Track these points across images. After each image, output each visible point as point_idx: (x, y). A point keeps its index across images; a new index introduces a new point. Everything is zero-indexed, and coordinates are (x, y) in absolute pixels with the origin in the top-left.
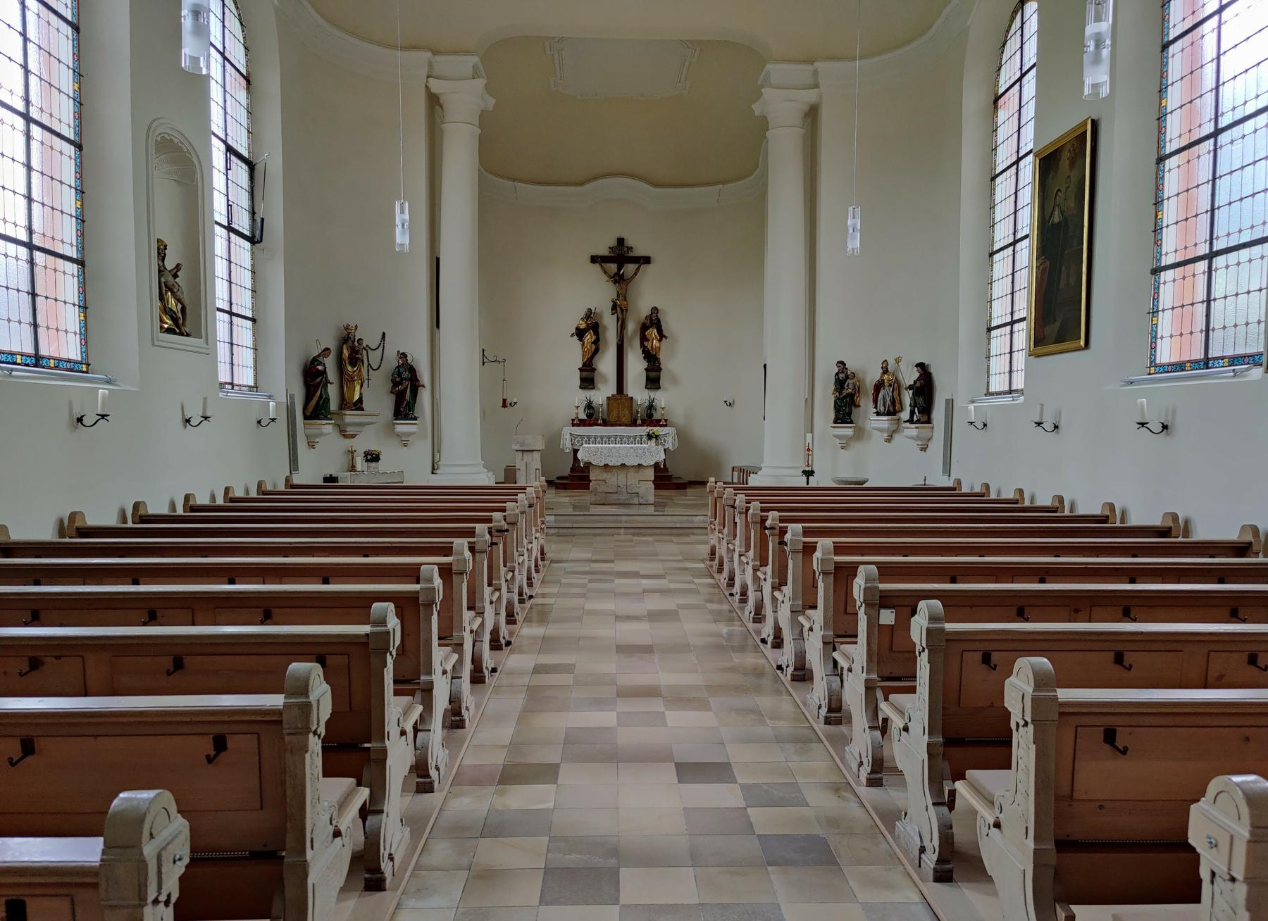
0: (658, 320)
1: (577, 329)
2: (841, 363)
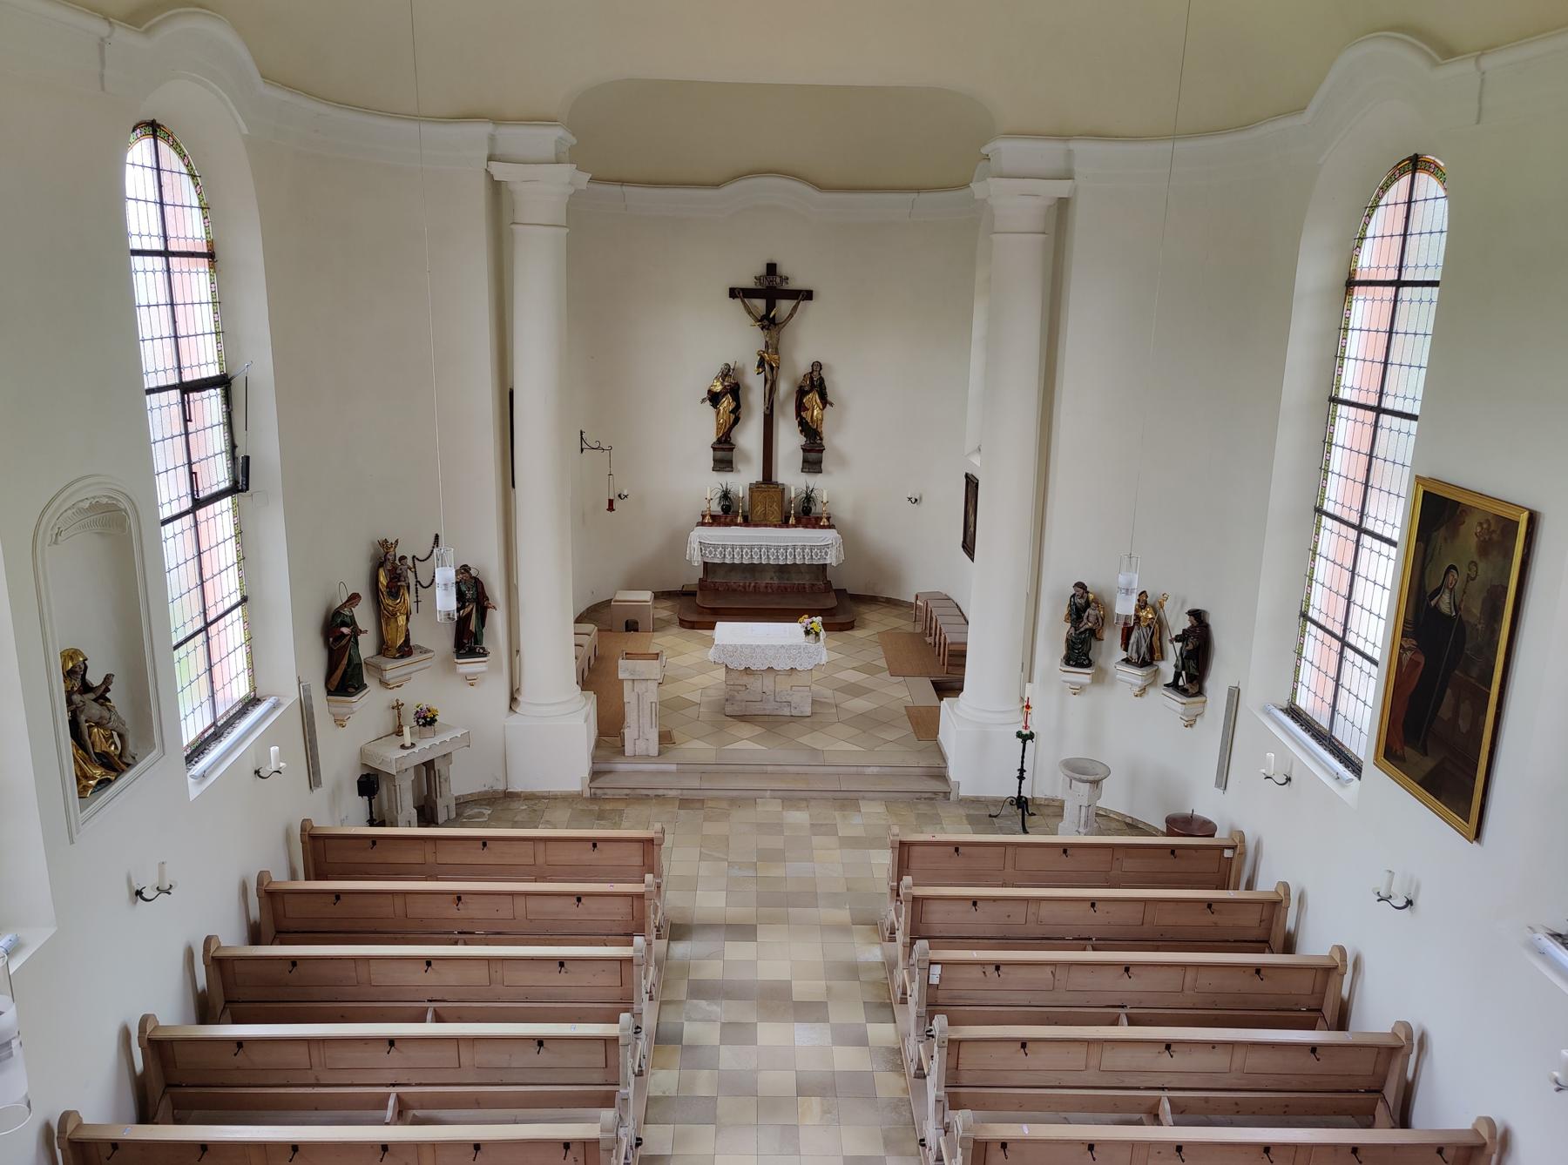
0: (822, 380)
1: (709, 391)
2: (1080, 586)
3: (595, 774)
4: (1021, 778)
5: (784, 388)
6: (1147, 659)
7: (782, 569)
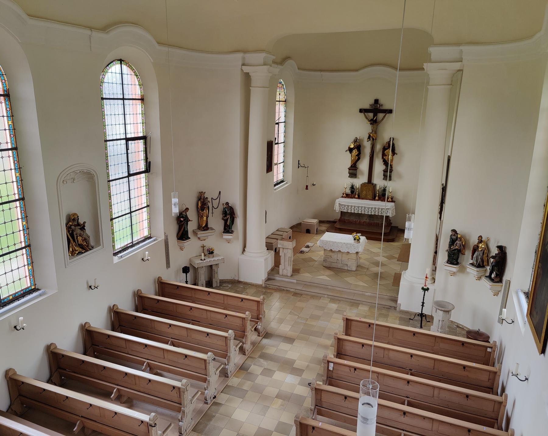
2: (454, 231)
3: (268, 279)
4: (423, 306)
5: (379, 147)
6: (480, 265)
7: (371, 216)
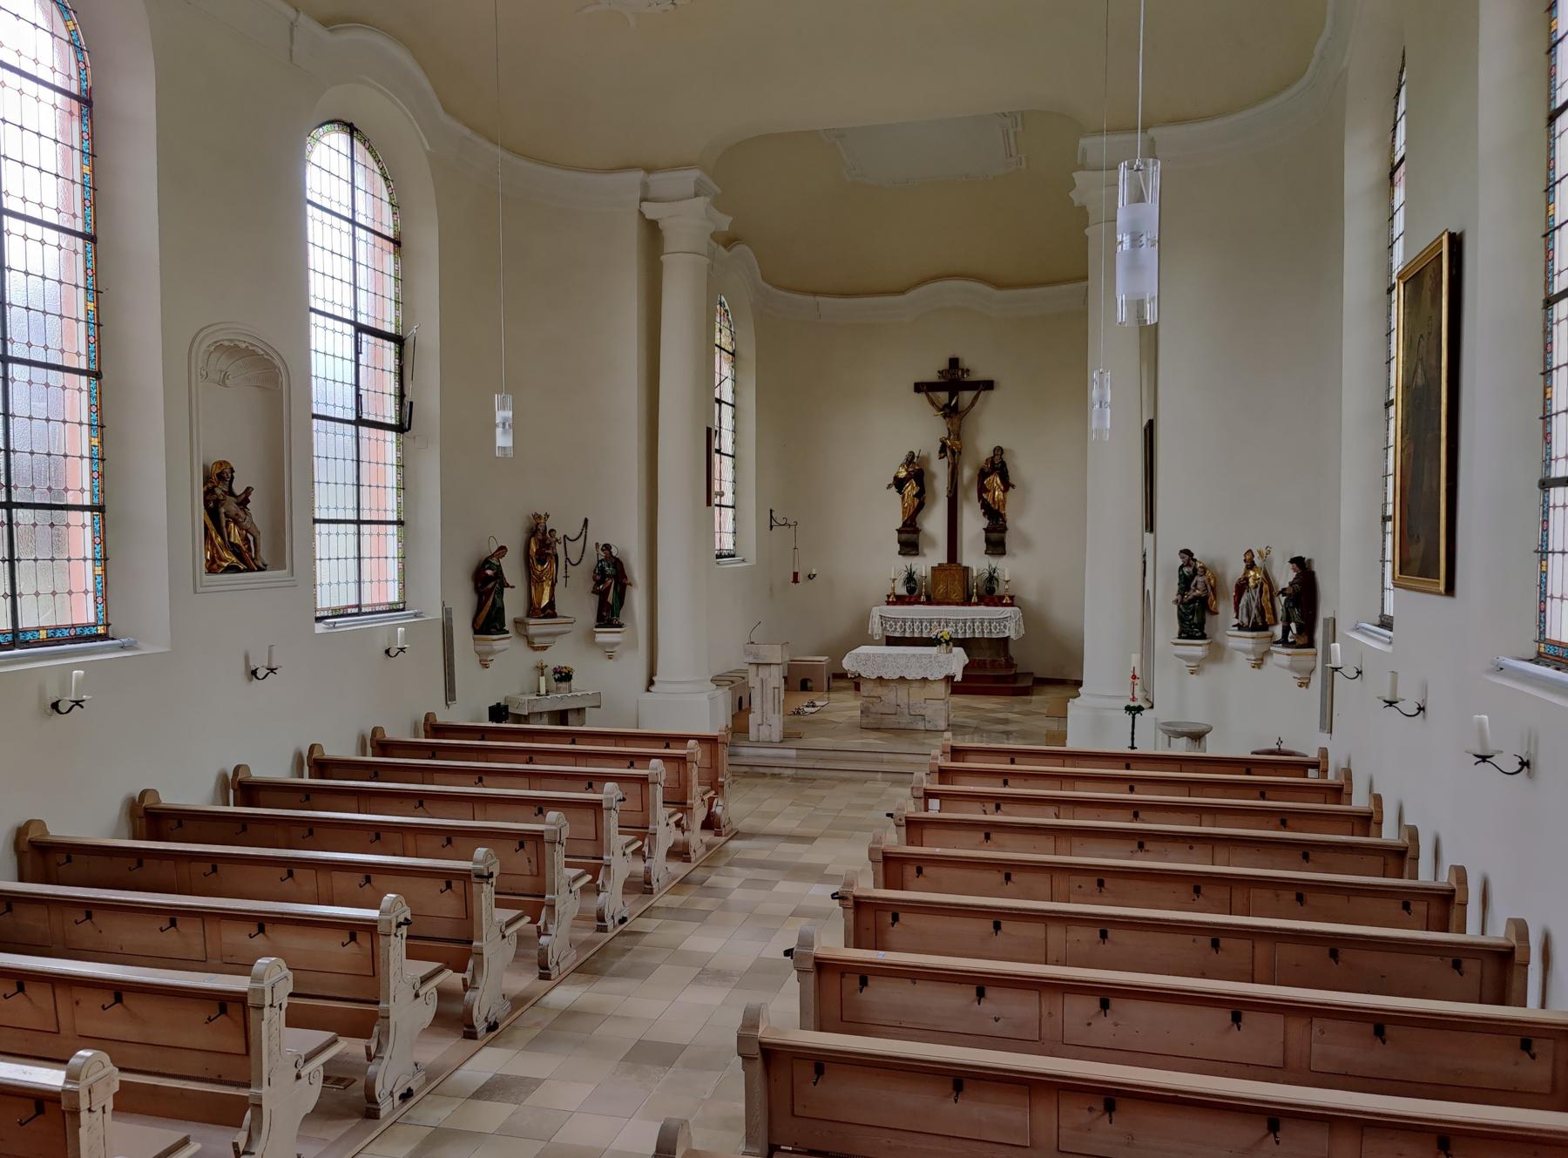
0: (1003, 464)
1: (896, 478)
2: (1187, 553)
5: (967, 474)
6: (1258, 625)
